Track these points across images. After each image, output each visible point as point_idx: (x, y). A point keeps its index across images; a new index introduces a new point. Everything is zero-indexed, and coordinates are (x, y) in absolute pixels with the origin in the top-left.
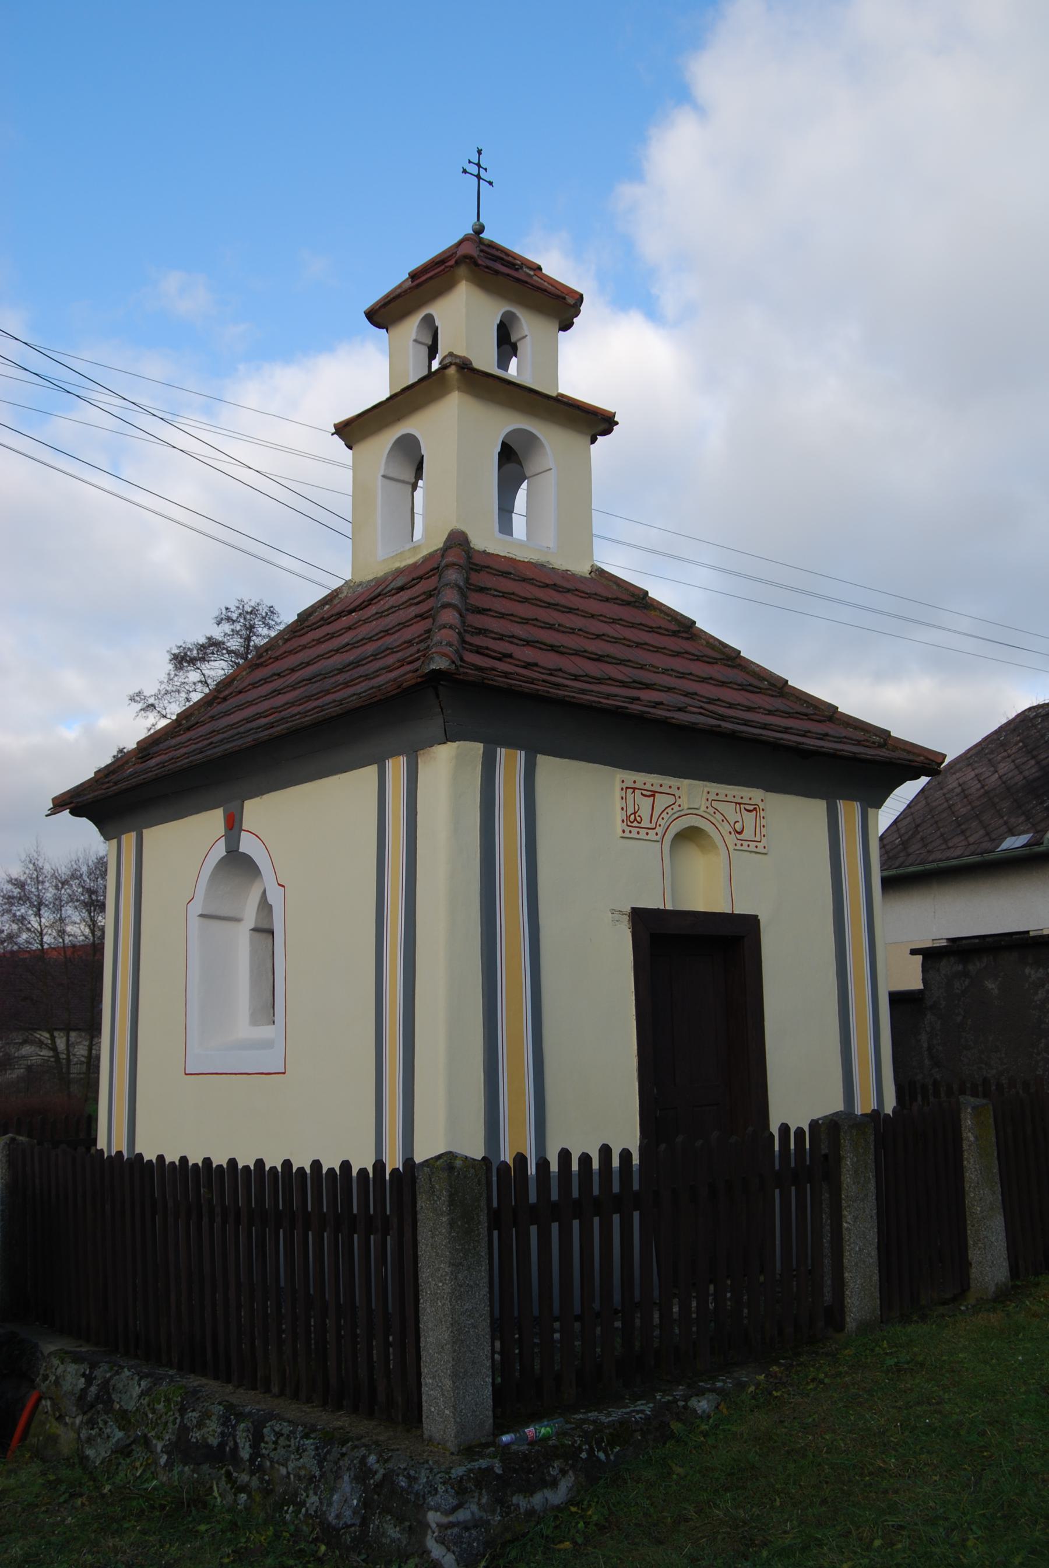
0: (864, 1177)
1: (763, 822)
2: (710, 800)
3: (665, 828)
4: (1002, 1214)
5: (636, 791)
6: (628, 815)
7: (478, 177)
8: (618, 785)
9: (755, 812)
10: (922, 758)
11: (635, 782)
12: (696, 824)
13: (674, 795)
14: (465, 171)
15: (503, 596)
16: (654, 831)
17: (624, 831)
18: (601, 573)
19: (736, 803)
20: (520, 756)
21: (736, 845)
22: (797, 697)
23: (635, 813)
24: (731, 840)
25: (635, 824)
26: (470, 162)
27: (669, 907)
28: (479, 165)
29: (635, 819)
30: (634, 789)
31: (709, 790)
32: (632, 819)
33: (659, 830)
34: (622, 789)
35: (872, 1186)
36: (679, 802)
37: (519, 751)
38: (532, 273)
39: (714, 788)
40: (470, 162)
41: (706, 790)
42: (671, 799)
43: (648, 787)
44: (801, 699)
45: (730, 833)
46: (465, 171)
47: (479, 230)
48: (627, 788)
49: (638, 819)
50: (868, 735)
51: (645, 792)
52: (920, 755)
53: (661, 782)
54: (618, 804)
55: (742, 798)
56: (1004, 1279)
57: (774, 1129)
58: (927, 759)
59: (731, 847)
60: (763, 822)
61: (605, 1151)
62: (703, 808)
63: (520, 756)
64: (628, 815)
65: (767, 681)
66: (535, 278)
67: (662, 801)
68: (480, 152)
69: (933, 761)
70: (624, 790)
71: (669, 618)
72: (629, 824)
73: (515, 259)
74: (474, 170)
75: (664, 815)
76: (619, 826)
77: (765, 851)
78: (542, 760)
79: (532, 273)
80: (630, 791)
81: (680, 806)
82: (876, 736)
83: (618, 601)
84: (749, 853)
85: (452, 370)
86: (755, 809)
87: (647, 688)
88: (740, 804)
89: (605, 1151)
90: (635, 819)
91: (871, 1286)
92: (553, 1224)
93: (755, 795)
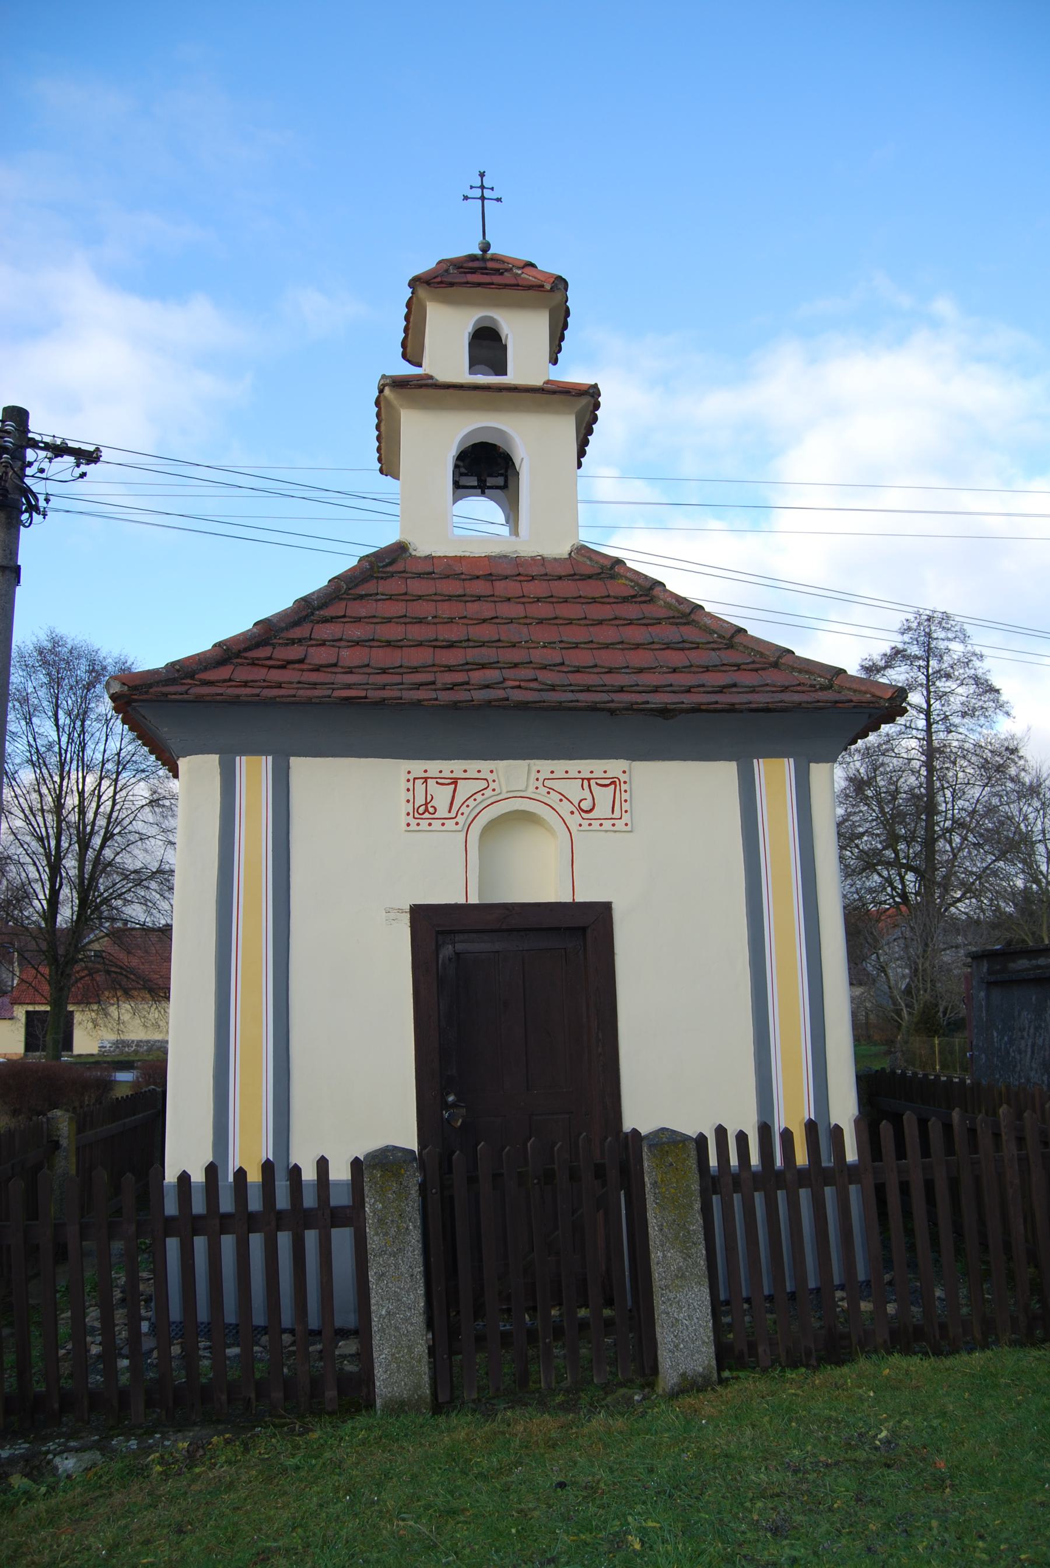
0: (398, 1227)
1: (625, 796)
2: (541, 780)
3: (470, 820)
4: (707, 1284)
5: (429, 781)
6: (416, 807)
7: (483, 198)
8: (404, 776)
9: (613, 786)
10: (869, 696)
11: (452, 772)
12: (515, 808)
13: (486, 779)
14: (466, 198)
15: (390, 599)
16: (454, 821)
17: (408, 825)
18: (582, 550)
19: (583, 779)
20: (265, 764)
21: (580, 825)
22: (745, 646)
23: (426, 804)
24: (574, 821)
25: (427, 815)
26: (472, 187)
27: (474, 900)
28: (482, 187)
29: (426, 810)
30: (426, 779)
31: (539, 768)
32: (425, 810)
33: (460, 819)
34: (408, 780)
35: (415, 1238)
36: (492, 785)
37: (264, 757)
38: (519, 272)
39: (545, 766)
40: (472, 187)
41: (534, 769)
42: (484, 784)
43: (446, 774)
44: (748, 648)
45: (572, 813)
46: (466, 198)
47: (486, 247)
48: (415, 779)
49: (431, 810)
50: (812, 677)
51: (440, 781)
52: (866, 693)
53: (464, 768)
54: (404, 795)
55: (579, 772)
56: (701, 1369)
57: (171, 1176)
58: (873, 696)
59: (574, 828)
60: (625, 796)
61: (721, 1132)
62: (532, 789)
63: (265, 764)
64: (416, 807)
65: (716, 633)
66: (524, 276)
67: (465, 789)
68: (482, 175)
69: (881, 698)
70: (412, 781)
71: (633, 584)
72: (416, 815)
73: (504, 262)
74: (478, 193)
75: (471, 802)
76: (404, 820)
77: (628, 828)
78: (297, 764)
79: (519, 272)
80: (419, 782)
81: (494, 790)
82: (821, 677)
83: (577, 577)
84: (613, 833)
85: (387, 391)
86: (614, 783)
87: (483, 668)
88: (589, 780)
89: (721, 1132)
90: (426, 810)
91: (412, 1358)
92: (307, 1232)
93: (615, 767)
